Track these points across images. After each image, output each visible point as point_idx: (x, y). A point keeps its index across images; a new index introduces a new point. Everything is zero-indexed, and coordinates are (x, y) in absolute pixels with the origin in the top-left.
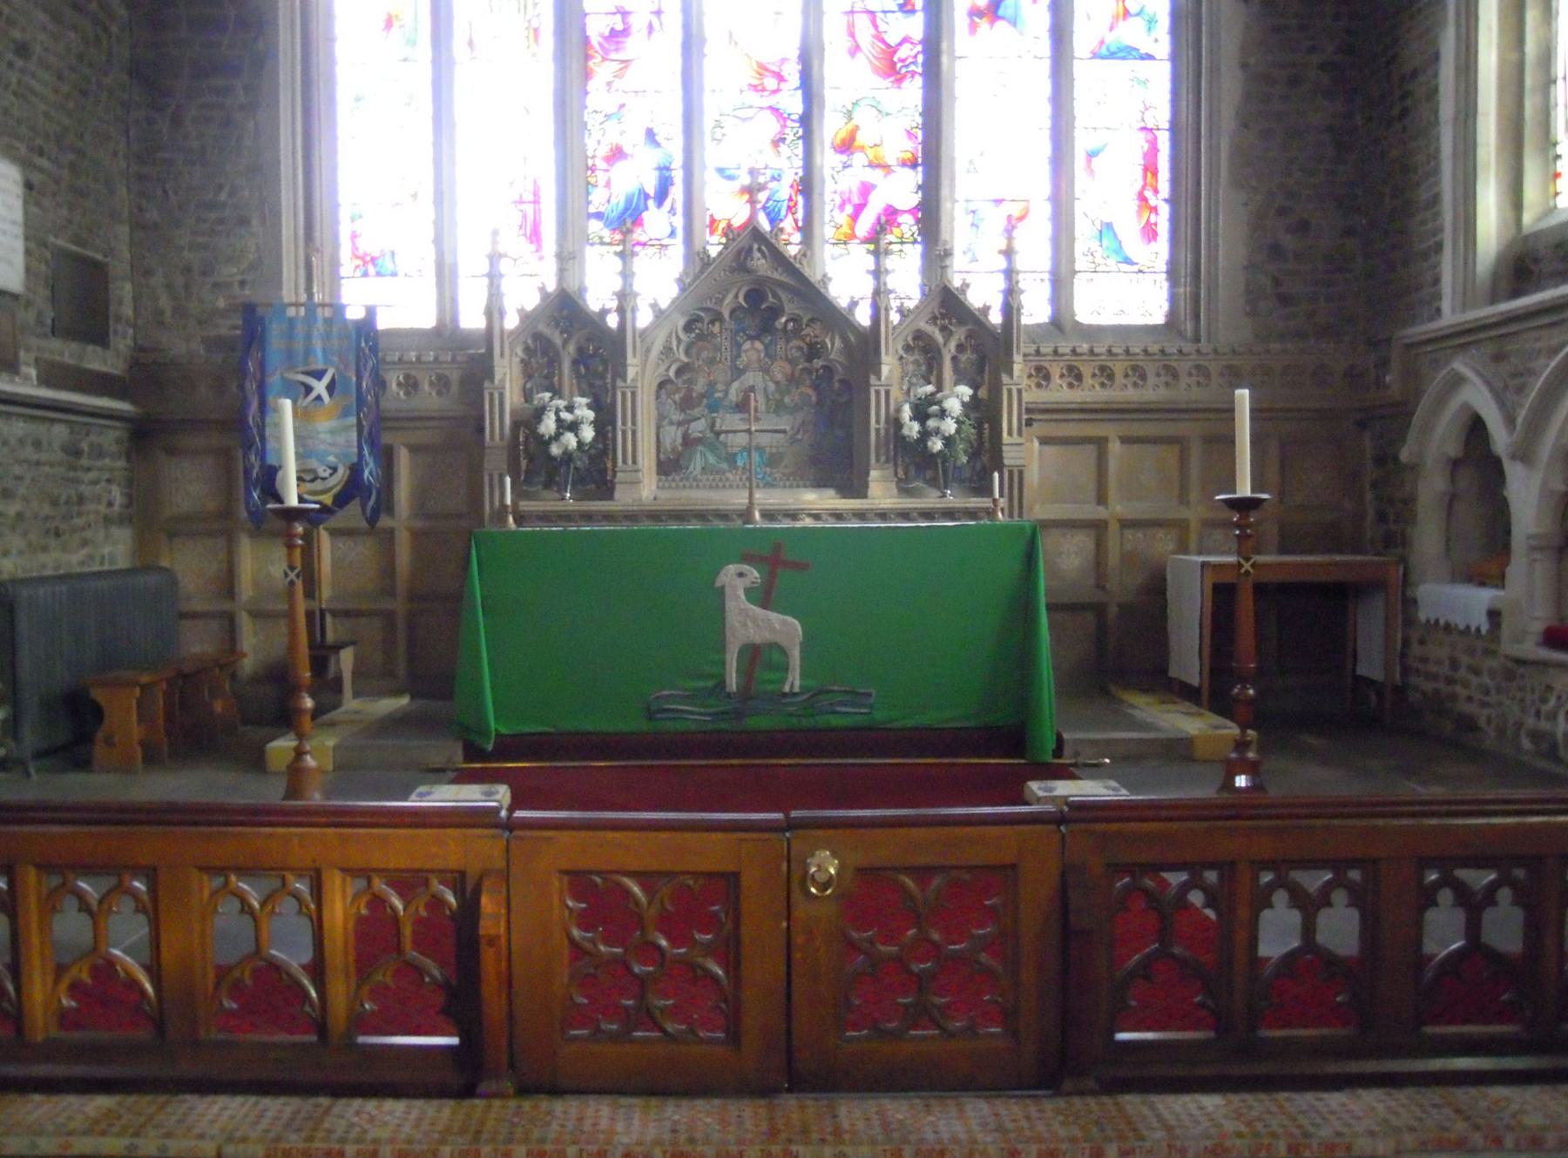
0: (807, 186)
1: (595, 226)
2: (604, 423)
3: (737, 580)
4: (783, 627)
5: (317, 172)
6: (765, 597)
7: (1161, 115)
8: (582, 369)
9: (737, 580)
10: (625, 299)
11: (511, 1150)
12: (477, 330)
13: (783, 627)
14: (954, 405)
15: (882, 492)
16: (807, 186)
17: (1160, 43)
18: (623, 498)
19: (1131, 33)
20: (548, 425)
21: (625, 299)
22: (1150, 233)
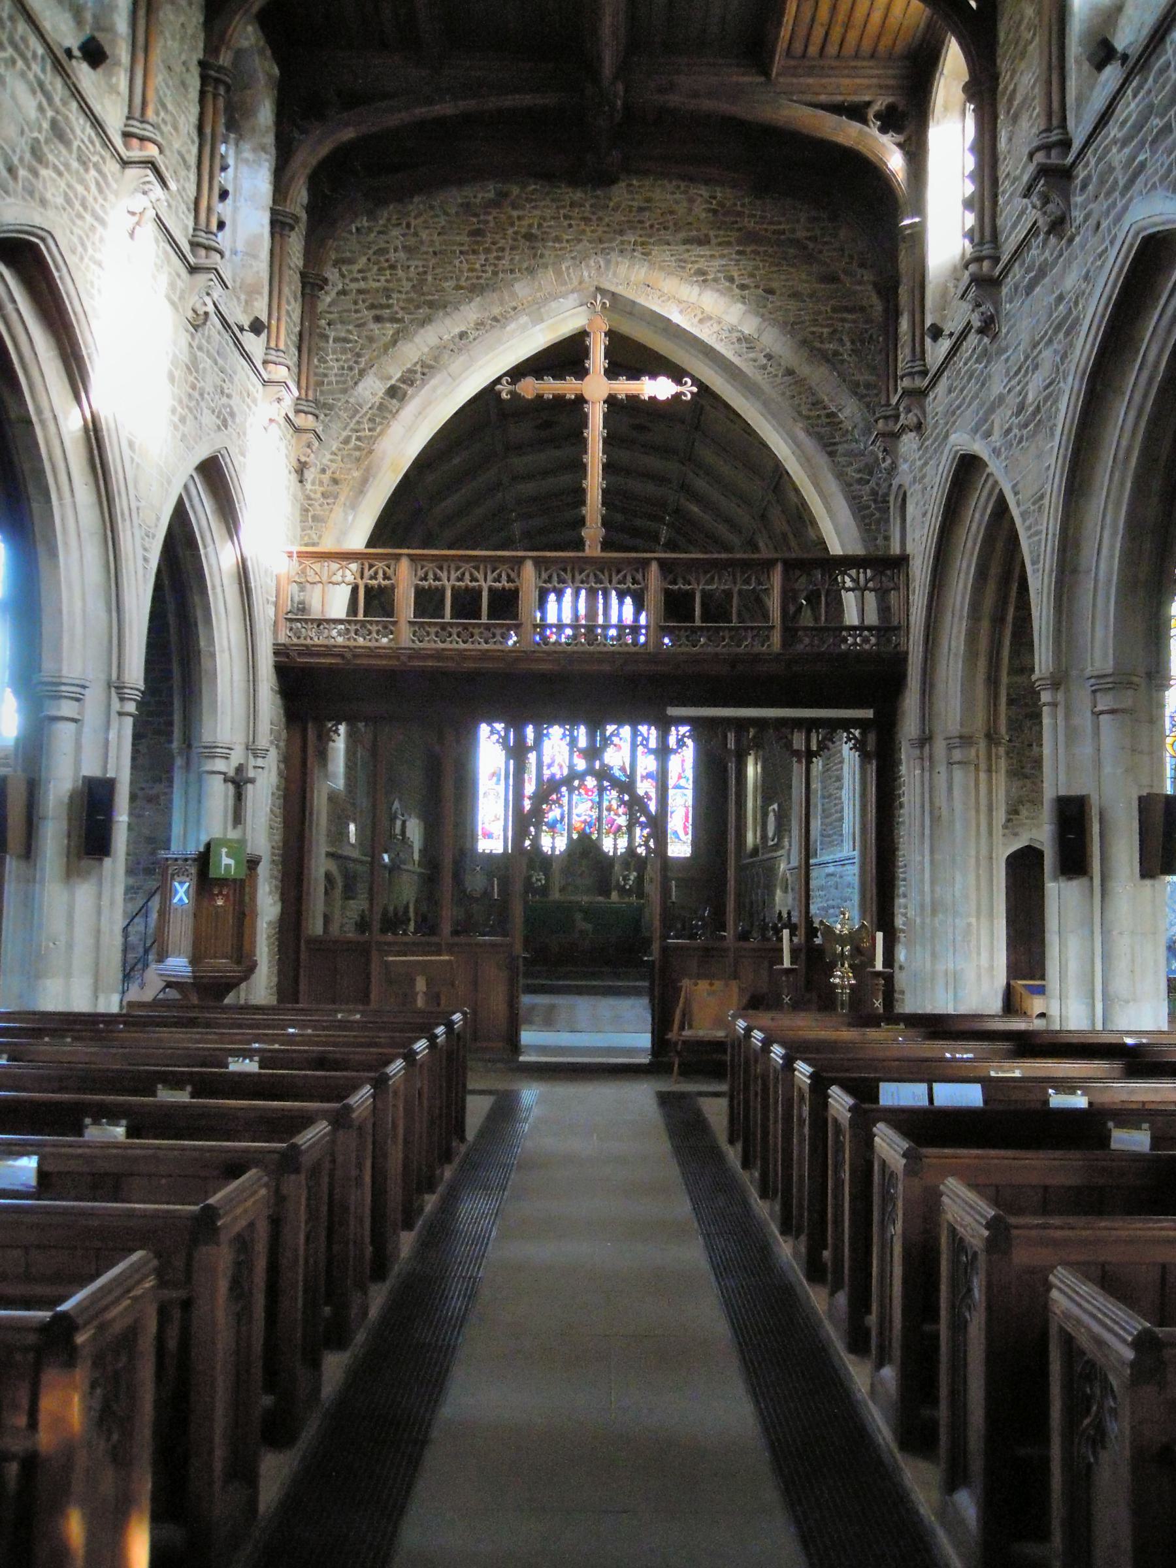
0: (599, 819)
1: (544, 828)
2: (547, 879)
3: (578, 916)
4: (588, 927)
5: (127, 648)
6: (585, 919)
7: (690, 803)
8: (626, 798)
9: (578, 916)
10: (553, 848)
11: (512, 1091)
12: (682, 855)
13: (588, 927)
14: (632, 877)
15: (614, 896)
16: (599, 819)
17: (690, 785)
18: (551, 898)
19: (682, 782)
20: (534, 879)
21: (553, 848)
22: (687, 834)
